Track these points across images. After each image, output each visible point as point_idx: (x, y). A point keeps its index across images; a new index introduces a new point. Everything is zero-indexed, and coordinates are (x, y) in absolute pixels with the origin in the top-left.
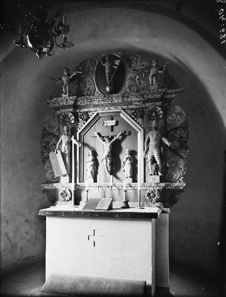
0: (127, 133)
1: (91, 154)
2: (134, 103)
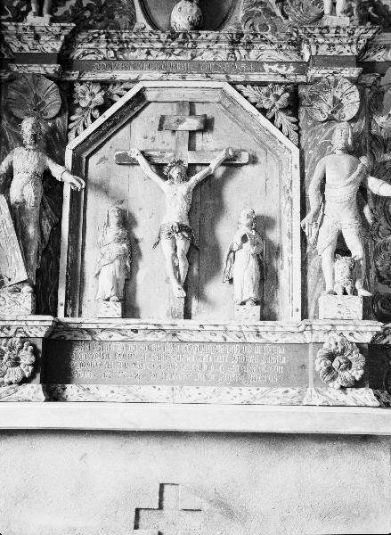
0: (244, 158)
1: (114, 220)
2: (266, 67)
